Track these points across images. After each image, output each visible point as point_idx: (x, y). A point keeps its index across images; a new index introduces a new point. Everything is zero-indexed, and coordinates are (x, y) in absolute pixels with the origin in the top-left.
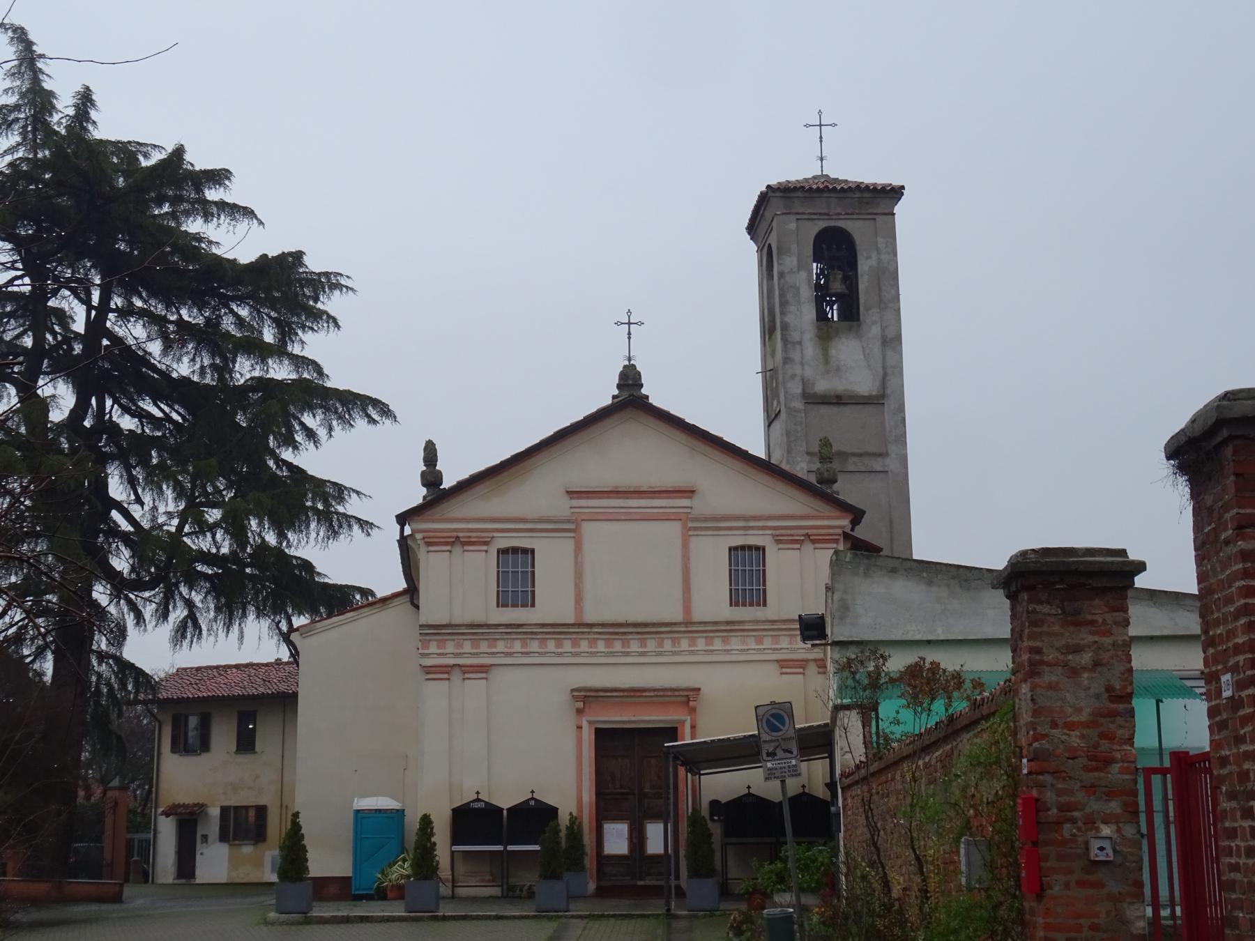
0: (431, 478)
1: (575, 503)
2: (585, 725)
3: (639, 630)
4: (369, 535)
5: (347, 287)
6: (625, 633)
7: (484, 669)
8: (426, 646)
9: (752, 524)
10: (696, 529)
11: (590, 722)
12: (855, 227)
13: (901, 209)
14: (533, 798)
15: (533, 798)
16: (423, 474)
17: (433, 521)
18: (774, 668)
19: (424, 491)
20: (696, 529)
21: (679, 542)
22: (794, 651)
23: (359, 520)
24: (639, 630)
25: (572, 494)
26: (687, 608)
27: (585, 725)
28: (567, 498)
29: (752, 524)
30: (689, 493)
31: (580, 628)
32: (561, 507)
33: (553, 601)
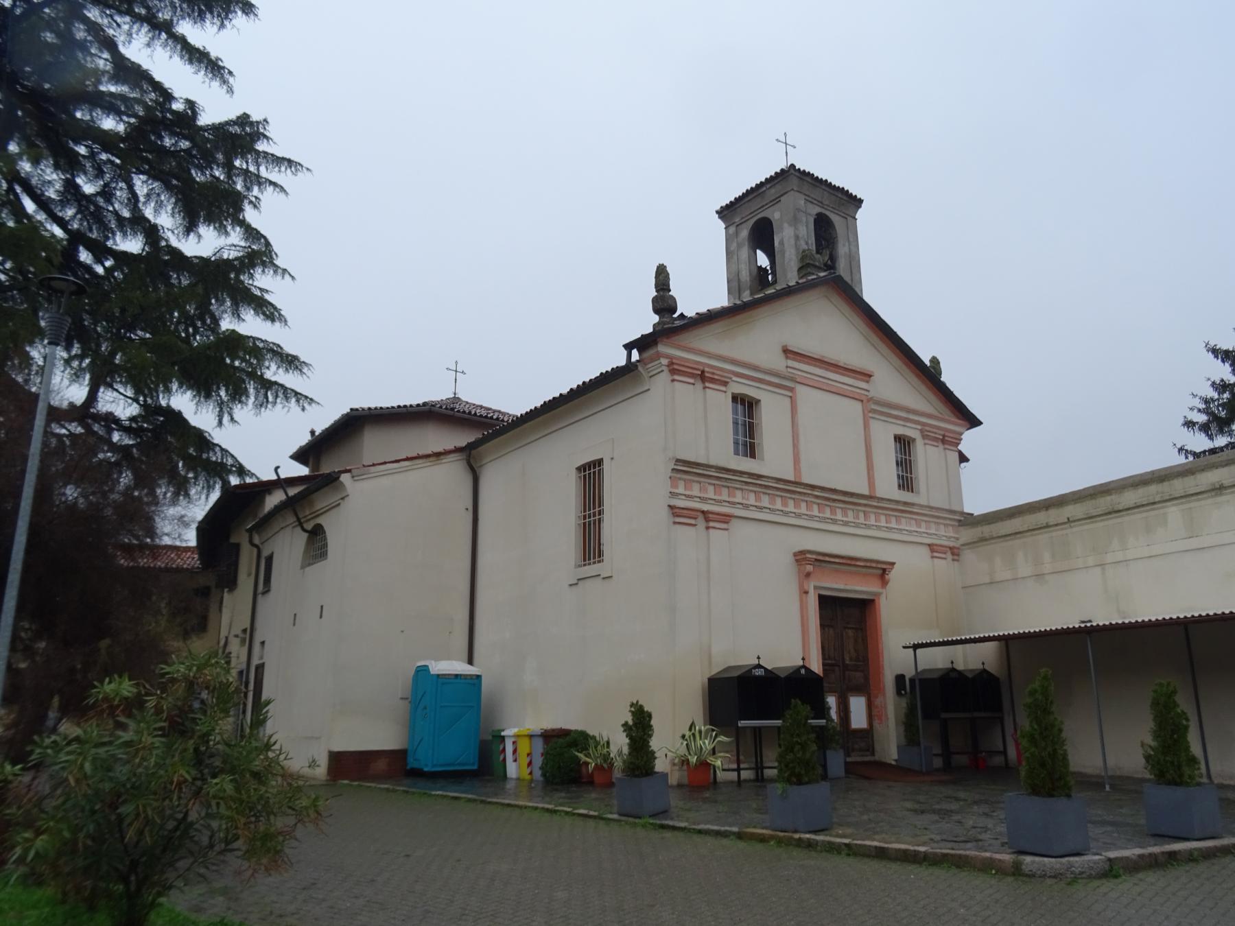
0: (664, 303)
1: (790, 363)
2: (811, 591)
3: (847, 499)
4: (303, 409)
5: (271, 183)
6: (834, 500)
7: (726, 519)
8: (674, 485)
9: (912, 417)
10: (875, 411)
11: (815, 588)
12: (835, 219)
13: (861, 215)
14: (804, 667)
15: (804, 667)
16: (655, 300)
17: (679, 347)
18: (925, 551)
19: (656, 318)
20: (875, 411)
21: (861, 422)
22: (939, 537)
23: (296, 393)
24: (847, 499)
25: (787, 352)
26: (871, 483)
27: (811, 591)
28: (782, 356)
29: (912, 417)
30: (867, 376)
31: (793, 488)
32: (779, 363)
33: (774, 459)
